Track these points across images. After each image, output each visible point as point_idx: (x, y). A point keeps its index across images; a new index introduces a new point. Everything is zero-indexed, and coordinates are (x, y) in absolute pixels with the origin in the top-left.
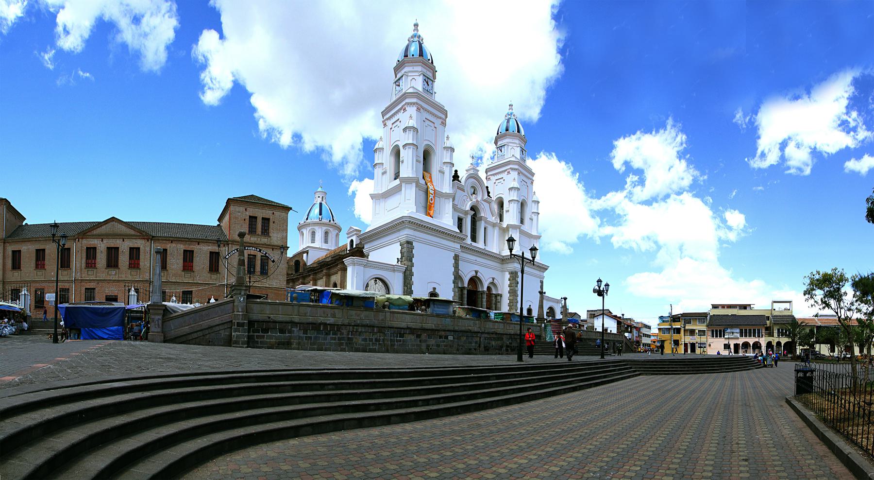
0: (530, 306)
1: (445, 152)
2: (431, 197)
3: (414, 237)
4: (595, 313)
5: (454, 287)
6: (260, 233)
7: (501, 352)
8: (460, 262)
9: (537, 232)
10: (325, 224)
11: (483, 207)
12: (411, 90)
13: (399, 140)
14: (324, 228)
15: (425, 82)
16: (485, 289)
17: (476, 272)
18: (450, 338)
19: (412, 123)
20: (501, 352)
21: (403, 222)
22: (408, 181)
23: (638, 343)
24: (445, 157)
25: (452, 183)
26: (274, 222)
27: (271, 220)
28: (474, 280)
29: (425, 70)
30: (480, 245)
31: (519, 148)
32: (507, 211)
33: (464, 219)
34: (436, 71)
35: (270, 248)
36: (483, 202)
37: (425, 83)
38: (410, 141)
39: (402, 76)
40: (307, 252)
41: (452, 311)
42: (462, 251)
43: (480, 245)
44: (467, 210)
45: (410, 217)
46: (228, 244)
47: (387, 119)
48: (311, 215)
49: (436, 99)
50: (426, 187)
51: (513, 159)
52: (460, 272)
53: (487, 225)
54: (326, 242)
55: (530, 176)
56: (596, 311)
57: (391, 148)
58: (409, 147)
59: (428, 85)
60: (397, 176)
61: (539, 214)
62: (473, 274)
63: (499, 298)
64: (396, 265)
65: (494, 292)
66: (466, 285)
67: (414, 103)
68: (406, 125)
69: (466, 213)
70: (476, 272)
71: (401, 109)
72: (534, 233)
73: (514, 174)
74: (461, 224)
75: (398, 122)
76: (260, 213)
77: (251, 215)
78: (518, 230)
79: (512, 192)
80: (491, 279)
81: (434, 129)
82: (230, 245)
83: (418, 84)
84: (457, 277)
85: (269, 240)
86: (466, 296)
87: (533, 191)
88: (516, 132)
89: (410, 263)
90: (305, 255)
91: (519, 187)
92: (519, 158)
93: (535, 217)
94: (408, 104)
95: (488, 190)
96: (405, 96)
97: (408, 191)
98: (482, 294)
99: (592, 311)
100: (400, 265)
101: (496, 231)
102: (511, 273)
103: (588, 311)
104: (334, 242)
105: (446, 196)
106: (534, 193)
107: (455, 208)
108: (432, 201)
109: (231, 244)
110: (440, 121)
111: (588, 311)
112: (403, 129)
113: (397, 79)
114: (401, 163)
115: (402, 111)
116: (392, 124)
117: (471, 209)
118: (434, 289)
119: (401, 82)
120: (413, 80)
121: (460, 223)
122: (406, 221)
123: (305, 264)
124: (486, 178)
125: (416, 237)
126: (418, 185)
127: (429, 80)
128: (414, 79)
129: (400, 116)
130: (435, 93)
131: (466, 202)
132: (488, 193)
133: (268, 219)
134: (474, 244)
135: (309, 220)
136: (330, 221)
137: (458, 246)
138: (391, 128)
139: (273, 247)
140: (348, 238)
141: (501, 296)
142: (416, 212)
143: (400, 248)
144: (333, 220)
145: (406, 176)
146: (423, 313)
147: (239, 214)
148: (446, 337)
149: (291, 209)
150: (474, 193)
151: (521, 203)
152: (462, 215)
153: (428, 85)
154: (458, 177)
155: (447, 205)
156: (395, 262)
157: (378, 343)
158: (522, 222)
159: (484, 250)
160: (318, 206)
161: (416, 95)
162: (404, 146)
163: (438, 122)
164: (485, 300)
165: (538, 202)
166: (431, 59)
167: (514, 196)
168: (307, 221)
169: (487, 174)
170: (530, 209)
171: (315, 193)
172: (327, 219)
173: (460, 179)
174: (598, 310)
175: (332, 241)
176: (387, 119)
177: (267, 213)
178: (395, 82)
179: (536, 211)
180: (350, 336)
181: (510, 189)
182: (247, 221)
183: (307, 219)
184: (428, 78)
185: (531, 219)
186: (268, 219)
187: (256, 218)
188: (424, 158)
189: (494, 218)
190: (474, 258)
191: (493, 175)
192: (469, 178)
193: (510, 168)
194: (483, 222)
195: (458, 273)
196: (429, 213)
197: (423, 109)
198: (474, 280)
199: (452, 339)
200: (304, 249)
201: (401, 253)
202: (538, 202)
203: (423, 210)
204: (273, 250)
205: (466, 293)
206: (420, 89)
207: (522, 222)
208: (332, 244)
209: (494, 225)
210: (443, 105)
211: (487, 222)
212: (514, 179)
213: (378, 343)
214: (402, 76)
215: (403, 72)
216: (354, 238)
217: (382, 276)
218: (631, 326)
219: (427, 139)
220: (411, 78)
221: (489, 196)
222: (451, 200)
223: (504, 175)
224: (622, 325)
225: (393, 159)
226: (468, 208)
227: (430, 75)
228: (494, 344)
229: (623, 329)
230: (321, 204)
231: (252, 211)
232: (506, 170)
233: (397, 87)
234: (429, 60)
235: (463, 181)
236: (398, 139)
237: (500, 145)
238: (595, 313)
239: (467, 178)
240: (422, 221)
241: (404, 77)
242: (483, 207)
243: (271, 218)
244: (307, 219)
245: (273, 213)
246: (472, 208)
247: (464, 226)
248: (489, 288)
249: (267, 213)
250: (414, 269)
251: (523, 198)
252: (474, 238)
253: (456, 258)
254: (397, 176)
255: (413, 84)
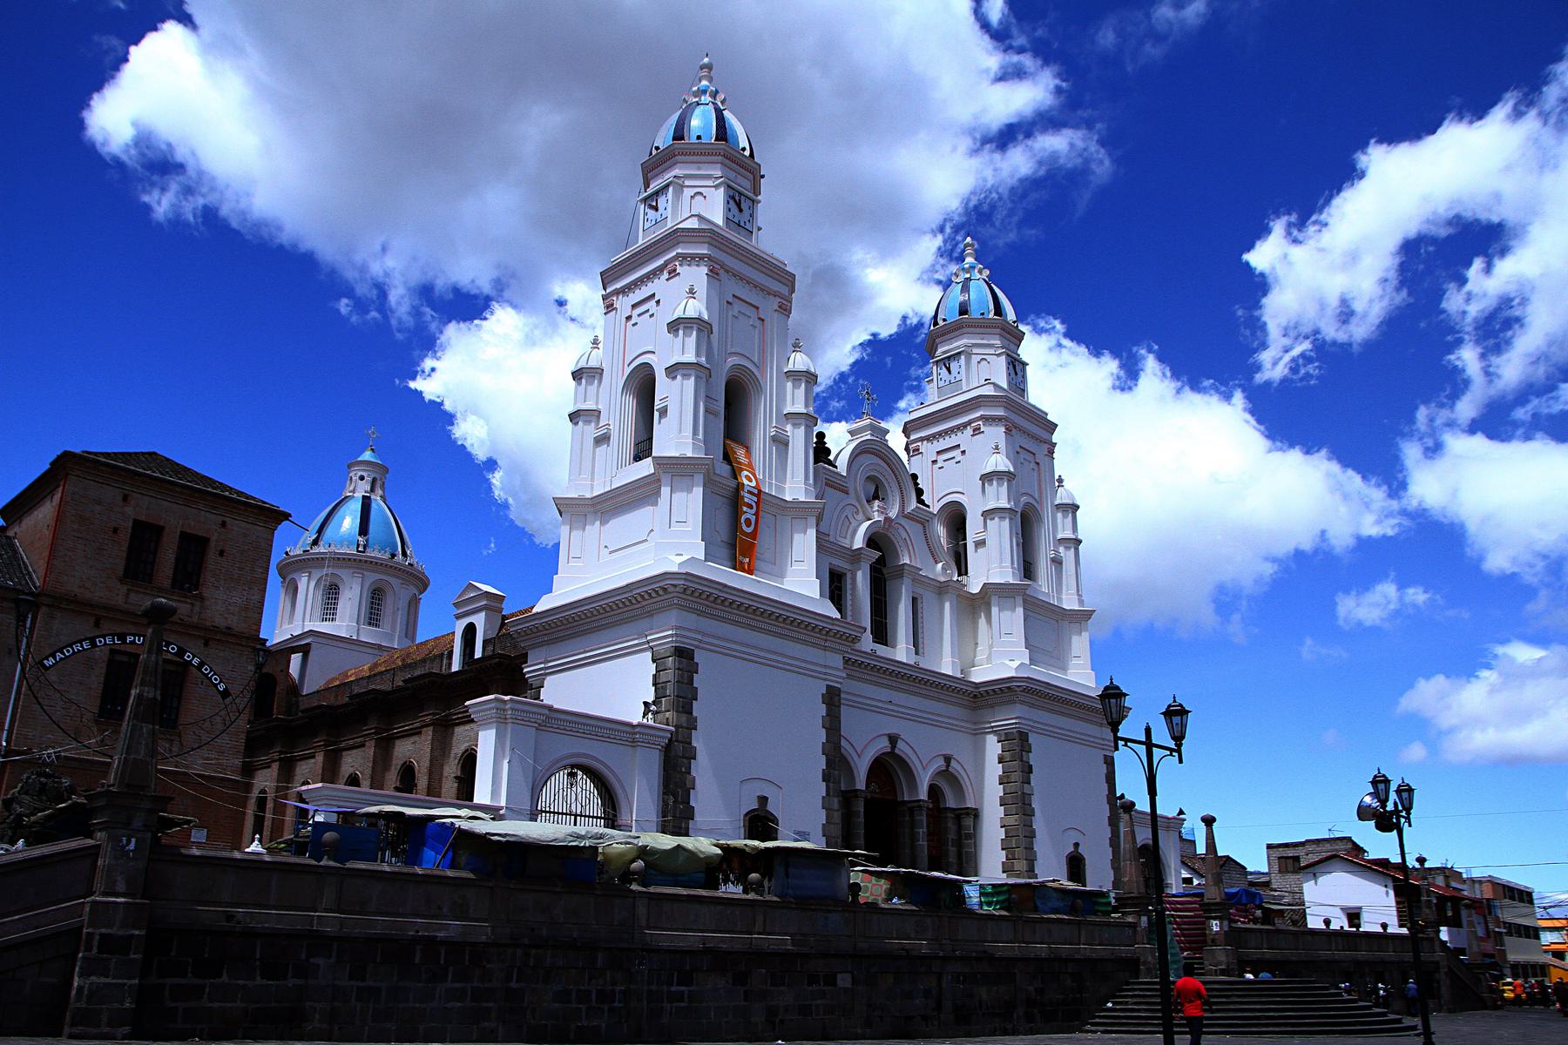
0: (1076, 845)
1: (789, 385)
2: (748, 514)
3: (1100, 741)
4: (1300, 852)
5: (828, 794)
6: (167, 583)
7: (1009, 1026)
8: (845, 713)
9: (1081, 602)
10: (374, 565)
11: (904, 535)
12: (693, 224)
13: (654, 353)
14: (372, 577)
15: (731, 202)
16: (923, 794)
17: (893, 740)
18: (844, 981)
19: (696, 308)
20: (1009, 1026)
21: (665, 589)
22: (675, 469)
23: (1495, 965)
24: (789, 397)
25: (815, 469)
26: (222, 553)
27: (212, 544)
28: (889, 768)
29: (732, 175)
30: (902, 651)
31: (1003, 358)
32: (980, 544)
33: (849, 576)
34: (763, 177)
35: (200, 637)
36: (903, 522)
37: (732, 205)
38: (690, 357)
39: (667, 186)
40: (305, 650)
41: (846, 887)
42: (849, 676)
43: (902, 651)
44: (855, 547)
45: (687, 574)
46: (38, 607)
47: (617, 292)
48: (329, 532)
49: (762, 246)
50: (733, 483)
51: (989, 391)
52: (843, 742)
53: (921, 591)
54: (373, 618)
55: (1044, 435)
56: (1302, 844)
57: (628, 370)
58: (685, 372)
59: (741, 210)
60: (643, 449)
61: (1080, 542)
62: (884, 745)
63: (969, 821)
64: (640, 725)
65: (951, 803)
66: (861, 784)
67: (701, 257)
68: (679, 313)
69: (855, 556)
70: (893, 740)
71: (661, 269)
72: (1069, 603)
73: (996, 434)
74: (840, 589)
75: (653, 303)
76: (175, 518)
77: (143, 518)
78: (1019, 600)
79: (991, 489)
80: (941, 762)
81: (757, 323)
82: (44, 609)
83: (714, 207)
84: (836, 762)
85: (197, 609)
86: (862, 820)
87: (1057, 477)
88: (991, 315)
89: (684, 718)
90: (296, 659)
91: (1012, 470)
92: (1005, 386)
93: (1067, 555)
94: (684, 258)
95: (916, 484)
96: (676, 236)
97: (679, 497)
98: (911, 810)
99: (1286, 845)
100: (651, 722)
101: (947, 605)
102: (1005, 737)
103: (1269, 847)
104: (400, 618)
105: (797, 510)
106: (1060, 480)
107: (823, 546)
108: (748, 526)
109: (48, 606)
110: (775, 303)
111: (1269, 847)
112: (668, 324)
113: (650, 191)
114: (656, 414)
115: (666, 275)
116: (634, 306)
117: (868, 545)
118: (763, 800)
119: (662, 202)
120: (699, 198)
121: (836, 587)
122: (675, 586)
123: (294, 689)
124: (907, 449)
125: (704, 634)
126: (709, 485)
127: (741, 201)
128: (701, 194)
129: (658, 286)
130: (759, 229)
131: (854, 523)
132: (920, 492)
133: (203, 542)
134: (882, 650)
135: (321, 549)
136: (393, 556)
137: (837, 660)
138: (629, 318)
139: (212, 636)
140: (458, 617)
141: (975, 814)
142: (705, 561)
143: (652, 668)
144: (404, 554)
145: (678, 455)
146: (751, 896)
147: (98, 508)
148: (831, 980)
149: (286, 516)
150: (876, 497)
151: (1022, 515)
152: (841, 564)
153: (741, 210)
154: (828, 451)
155: (797, 537)
156: (635, 716)
157: (606, 1007)
158: (1028, 570)
159: (916, 667)
160: (355, 506)
161: (707, 234)
162: (672, 371)
163: (769, 306)
164: (922, 831)
165: (1075, 507)
166: (748, 148)
167: (999, 497)
168: (316, 550)
169: (907, 436)
170: (1054, 528)
171: (349, 467)
172: (382, 549)
173: (831, 457)
174: (1308, 841)
175: (394, 622)
176: (617, 292)
177: (203, 521)
178: (645, 200)
179: (1069, 534)
180: (513, 985)
181: (987, 478)
182: (125, 536)
183: (315, 543)
184: (740, 194)
185: (1057, 562)
186: (203, 542)
187: (157, 531)
188: (728, 404)
189: (940, 565)
190: (883, 694)
191: (928, 439)
192: (865, 452)
193: (981, 418)
194: (907, 581)
195: (838, 747)
196: (742, 563)
197: (727, 271)
198: (889, 768)
199: (849, 985)
200: (293, 637)
201: (655, 684)
202: (1075, 507)
203: (724, 552)
204: (206, 644)
205: (862, 810)
206: (719, 220)
207: (1028, 570)
208: (393, 628)
209: (942, 589)
210: (782, 259)
211: (918, 579)
212: (997, 447)
213: (606, 1007)
214: (667, 186)
215: (668, 176)
216: (479, 620)
217: (593, 757)
218: (1456, 900)
219: (733, 350)
220: (693, 191)
221: (922, 502)
222: (813, 521)
223: (963, 438)
224: (1424, 898)
225: (630, 403)
226: (859, 542)
227: (744, 185)
228: (984, 996)
229: (1429, 914)
230: (366, 504)
231: (145, 507)
232: (969, 423)
233: (651, 213)
234: (744, 149)
235: (842, 465)
236: (650, 348)
237: (944, 353)
238: (1300, 852)
239: (855, 456)
240: (725, 586)
241: (671, 189)
242: (904, 535)
243: (214, 538)
244: (315, 543)
245: (224, 524)
246: (872, 541)
247: (849, 597)
248: (934, 791)
249: (203, 521)
250: (698, 741)
251: (1024, 499)
252: (882, 633)
253: (832, 698)
254: (643, 449)
255: (699, 206)
